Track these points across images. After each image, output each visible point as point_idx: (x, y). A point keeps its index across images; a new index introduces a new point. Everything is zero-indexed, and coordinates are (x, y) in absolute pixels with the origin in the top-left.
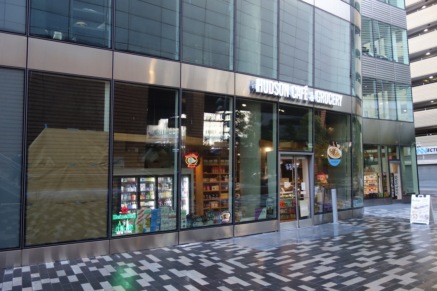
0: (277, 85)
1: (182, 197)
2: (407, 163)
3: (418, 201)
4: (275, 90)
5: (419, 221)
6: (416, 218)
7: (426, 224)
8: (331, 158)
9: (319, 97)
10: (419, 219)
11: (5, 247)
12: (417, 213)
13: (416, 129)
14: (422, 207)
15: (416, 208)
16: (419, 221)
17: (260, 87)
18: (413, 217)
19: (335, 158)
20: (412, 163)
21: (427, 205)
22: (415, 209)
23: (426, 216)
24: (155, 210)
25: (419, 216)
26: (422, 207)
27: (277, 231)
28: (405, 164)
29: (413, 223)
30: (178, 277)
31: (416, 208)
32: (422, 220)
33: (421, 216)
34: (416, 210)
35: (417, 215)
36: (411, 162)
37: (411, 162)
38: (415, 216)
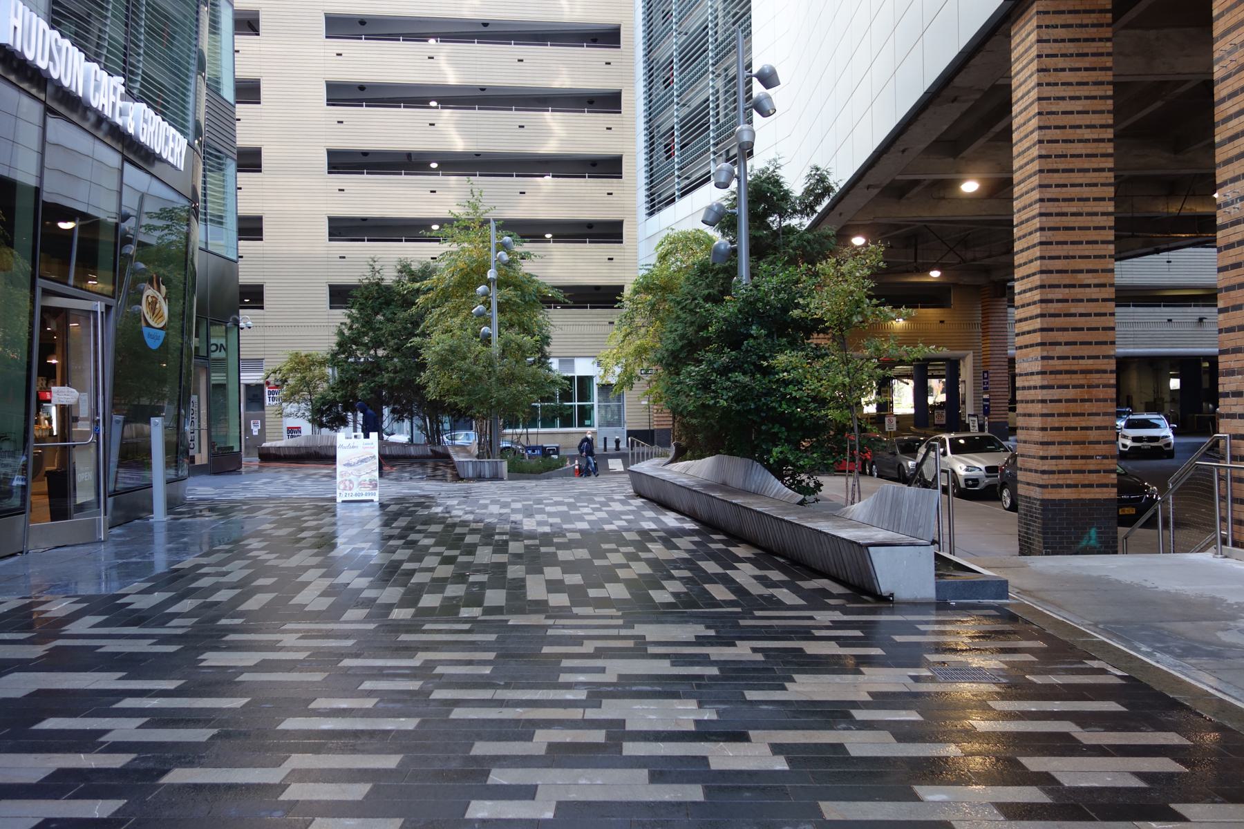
0: (56, 40)
1: (369, 274)
2: (217, 378)
3: (353, 447)
4: (51, 58)
5: (356, 495)
6: (351, 489)
7: (372, 501)
8: (148, 325)
9: (145, 126)
10: (355, 491)
11: (24, 383)
12: (352, 477)
13: (241, 286)
14: (362, 461)
15: (348, 465)
16: (356, 495)
17: (15, 28)
18: (342, 486)
19: (155, 325)
20: (227, 380)
21: (374, 457)
22: (346, 469)
23: (371, 481)
24: (958, 172)
25: (356, 484)
26: (362, 461)
27: (22, 552)
28: (213, 382)
29: (343, 502)
30: (715, 562)
31: (348, 465)
32: (364, 491)
33: (360, 484)
34: (350, 470)
35: (350, 481)
36: (227, 376)
37: (227, 376)
38: (347, 483)
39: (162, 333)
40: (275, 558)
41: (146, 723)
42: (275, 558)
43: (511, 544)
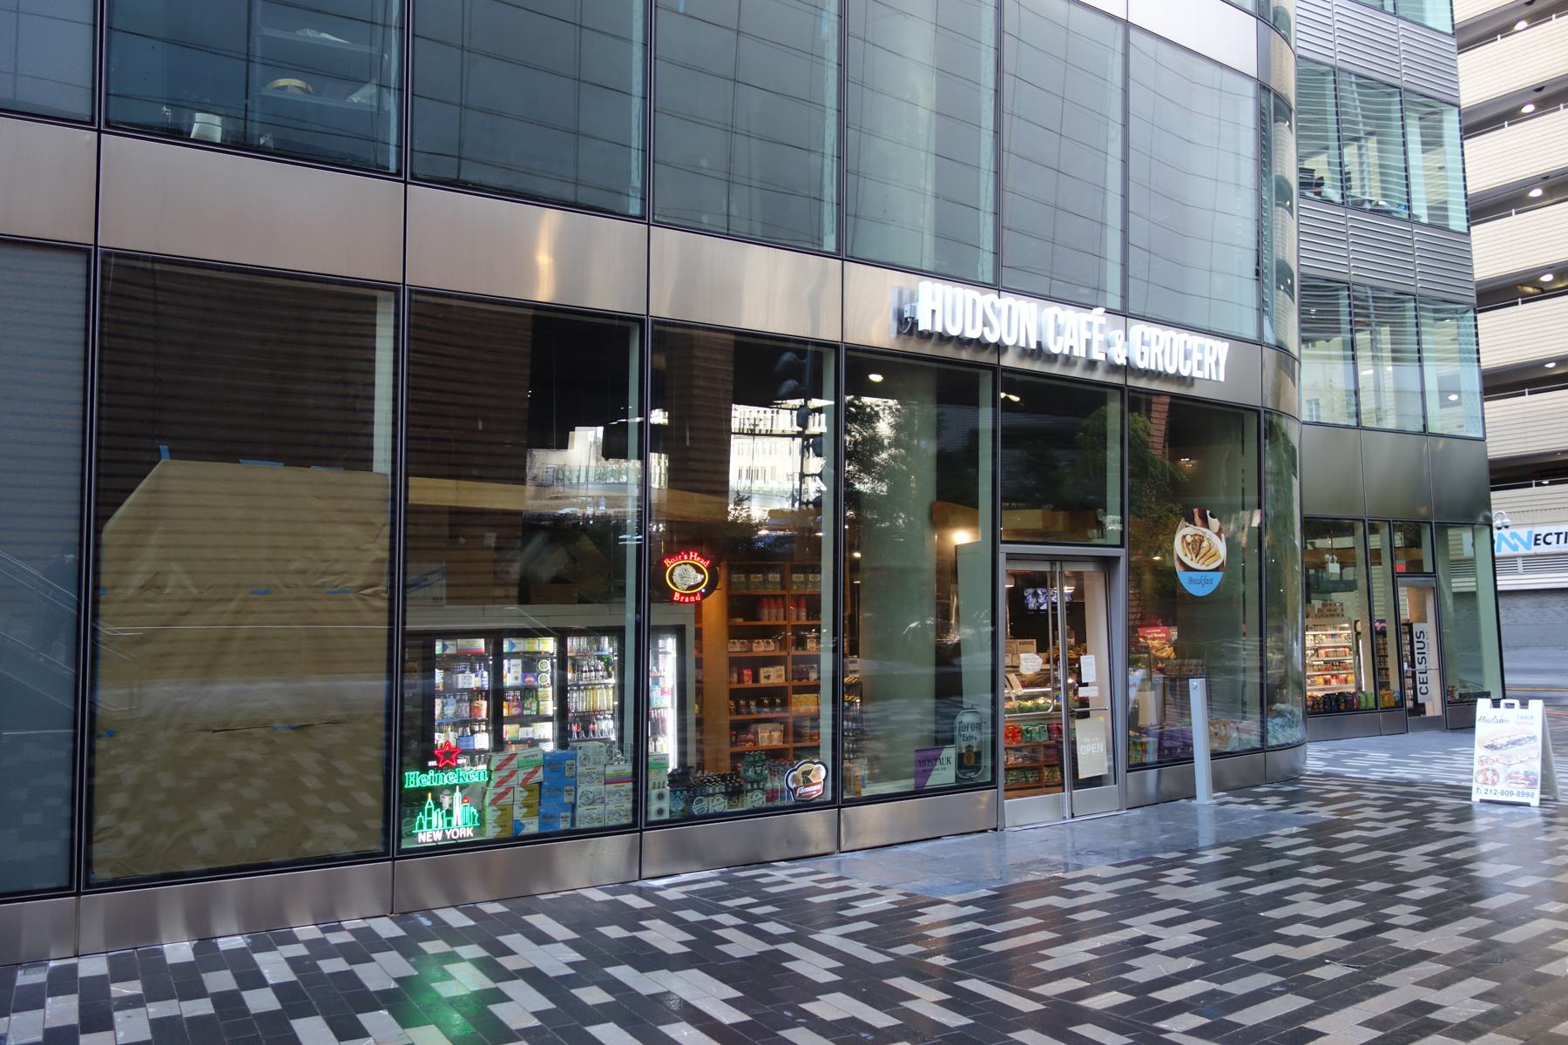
0: (992, 305)
1: (655, 706)
2: (1461, 584)
3: (1502, 721)
4: (986, 323)
5: (1503, 793)
6: (1494, 783)
7: (1528, 805)
8: (1188, 568)
10: (1502, 785)
12: (1497, 766)
14: (1514, 743)
15: (1492, 747)
16: (1503, 793)
17: (934, 311)
18: (1481, 778)
20: (1477, 586)
21: (1534, 738)
22: (1488, 752)
23: (1527, 775)
25: (1502, 776)
26: (1514, 743)
27: (995, 830)
28: (1454, 590)
29: (1482, 801)
31: (1492, 747)
32: (1515, 788)
33: (1509, 777)
34: (1494, 754)
35: (1494, 772)
36: (1476, 581)
37: (1476, 581)
38: (1489, 774)
39: (1218, 576)
40: (736, 927)
41: (1203, 1027)
42: (736, 927)
43: (73, 1019)
